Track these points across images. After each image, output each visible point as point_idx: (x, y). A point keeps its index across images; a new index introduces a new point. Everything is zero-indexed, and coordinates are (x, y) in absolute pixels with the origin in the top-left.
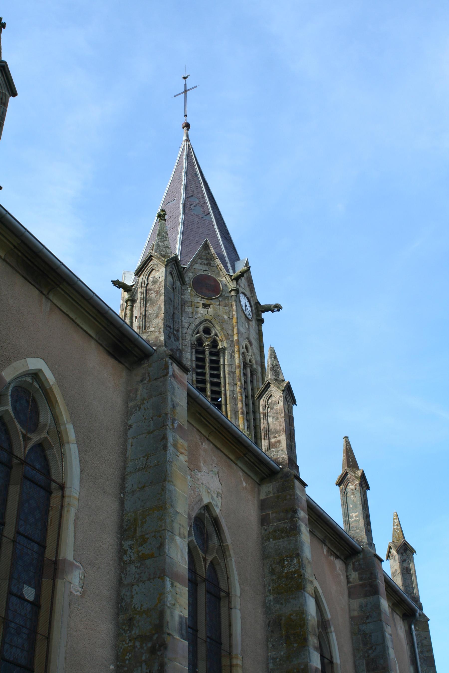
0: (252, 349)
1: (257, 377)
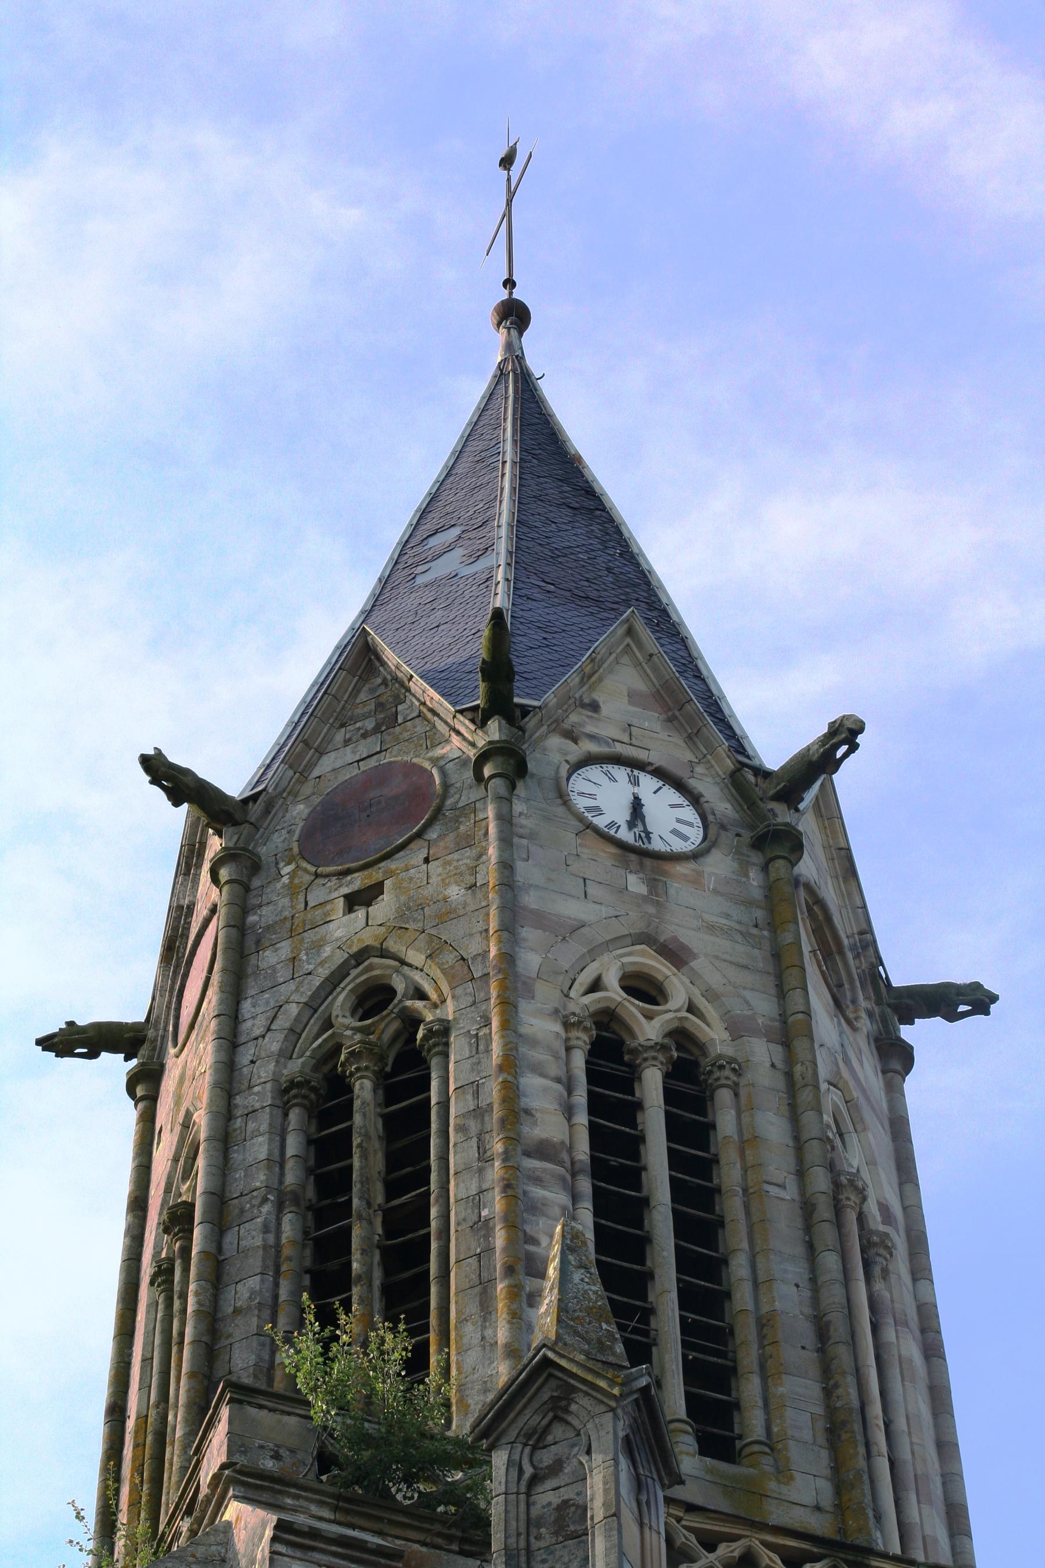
0: (694, 979)
1: (743, 1092)
